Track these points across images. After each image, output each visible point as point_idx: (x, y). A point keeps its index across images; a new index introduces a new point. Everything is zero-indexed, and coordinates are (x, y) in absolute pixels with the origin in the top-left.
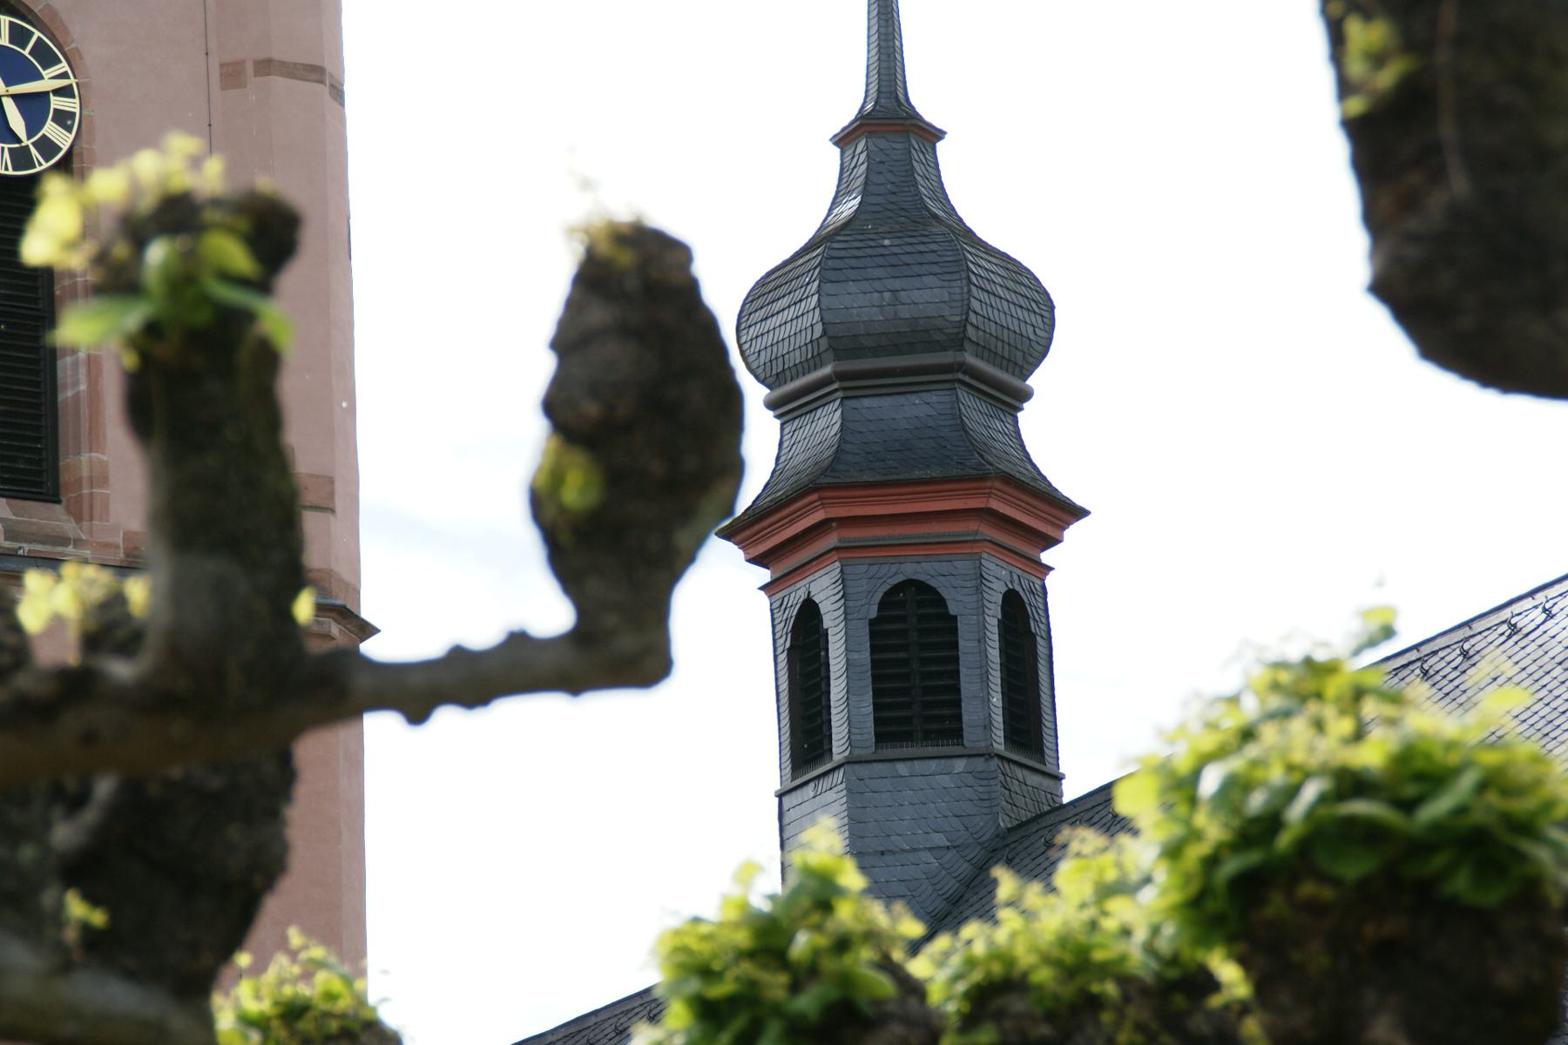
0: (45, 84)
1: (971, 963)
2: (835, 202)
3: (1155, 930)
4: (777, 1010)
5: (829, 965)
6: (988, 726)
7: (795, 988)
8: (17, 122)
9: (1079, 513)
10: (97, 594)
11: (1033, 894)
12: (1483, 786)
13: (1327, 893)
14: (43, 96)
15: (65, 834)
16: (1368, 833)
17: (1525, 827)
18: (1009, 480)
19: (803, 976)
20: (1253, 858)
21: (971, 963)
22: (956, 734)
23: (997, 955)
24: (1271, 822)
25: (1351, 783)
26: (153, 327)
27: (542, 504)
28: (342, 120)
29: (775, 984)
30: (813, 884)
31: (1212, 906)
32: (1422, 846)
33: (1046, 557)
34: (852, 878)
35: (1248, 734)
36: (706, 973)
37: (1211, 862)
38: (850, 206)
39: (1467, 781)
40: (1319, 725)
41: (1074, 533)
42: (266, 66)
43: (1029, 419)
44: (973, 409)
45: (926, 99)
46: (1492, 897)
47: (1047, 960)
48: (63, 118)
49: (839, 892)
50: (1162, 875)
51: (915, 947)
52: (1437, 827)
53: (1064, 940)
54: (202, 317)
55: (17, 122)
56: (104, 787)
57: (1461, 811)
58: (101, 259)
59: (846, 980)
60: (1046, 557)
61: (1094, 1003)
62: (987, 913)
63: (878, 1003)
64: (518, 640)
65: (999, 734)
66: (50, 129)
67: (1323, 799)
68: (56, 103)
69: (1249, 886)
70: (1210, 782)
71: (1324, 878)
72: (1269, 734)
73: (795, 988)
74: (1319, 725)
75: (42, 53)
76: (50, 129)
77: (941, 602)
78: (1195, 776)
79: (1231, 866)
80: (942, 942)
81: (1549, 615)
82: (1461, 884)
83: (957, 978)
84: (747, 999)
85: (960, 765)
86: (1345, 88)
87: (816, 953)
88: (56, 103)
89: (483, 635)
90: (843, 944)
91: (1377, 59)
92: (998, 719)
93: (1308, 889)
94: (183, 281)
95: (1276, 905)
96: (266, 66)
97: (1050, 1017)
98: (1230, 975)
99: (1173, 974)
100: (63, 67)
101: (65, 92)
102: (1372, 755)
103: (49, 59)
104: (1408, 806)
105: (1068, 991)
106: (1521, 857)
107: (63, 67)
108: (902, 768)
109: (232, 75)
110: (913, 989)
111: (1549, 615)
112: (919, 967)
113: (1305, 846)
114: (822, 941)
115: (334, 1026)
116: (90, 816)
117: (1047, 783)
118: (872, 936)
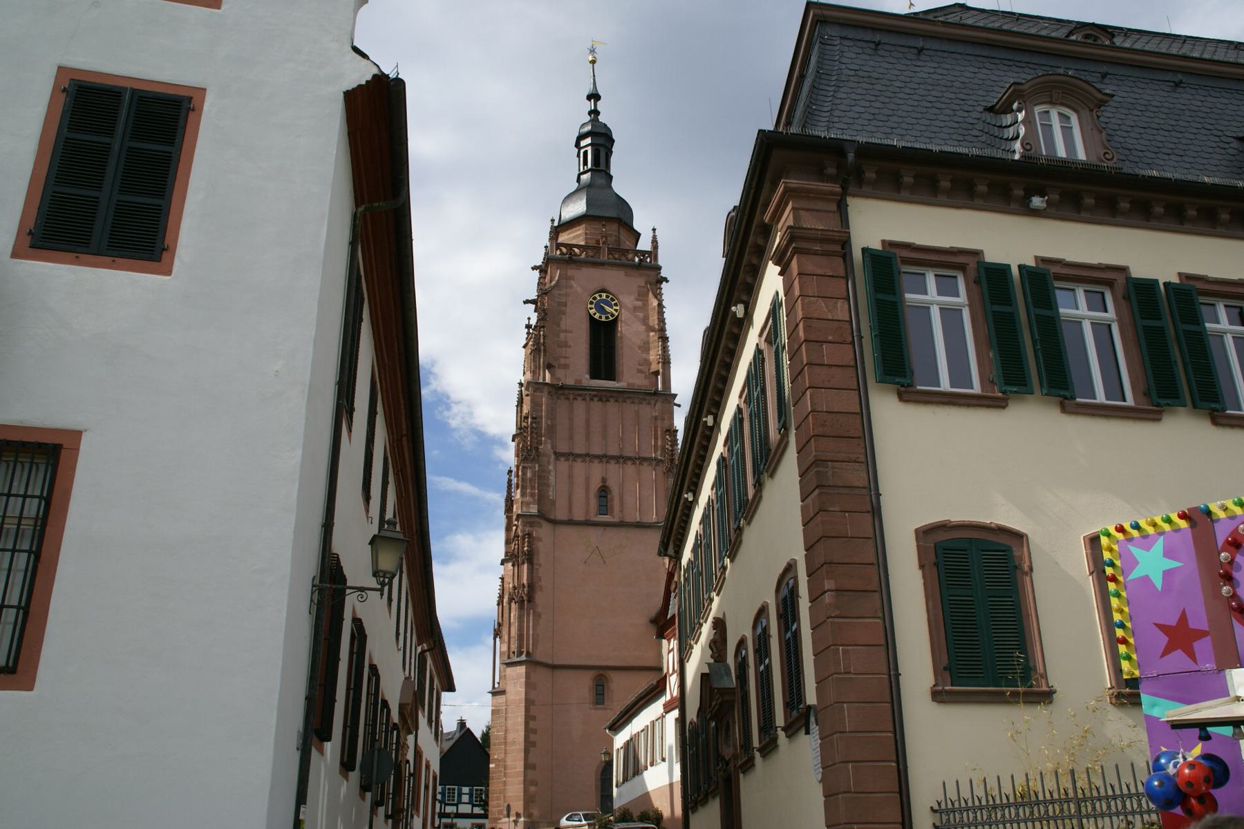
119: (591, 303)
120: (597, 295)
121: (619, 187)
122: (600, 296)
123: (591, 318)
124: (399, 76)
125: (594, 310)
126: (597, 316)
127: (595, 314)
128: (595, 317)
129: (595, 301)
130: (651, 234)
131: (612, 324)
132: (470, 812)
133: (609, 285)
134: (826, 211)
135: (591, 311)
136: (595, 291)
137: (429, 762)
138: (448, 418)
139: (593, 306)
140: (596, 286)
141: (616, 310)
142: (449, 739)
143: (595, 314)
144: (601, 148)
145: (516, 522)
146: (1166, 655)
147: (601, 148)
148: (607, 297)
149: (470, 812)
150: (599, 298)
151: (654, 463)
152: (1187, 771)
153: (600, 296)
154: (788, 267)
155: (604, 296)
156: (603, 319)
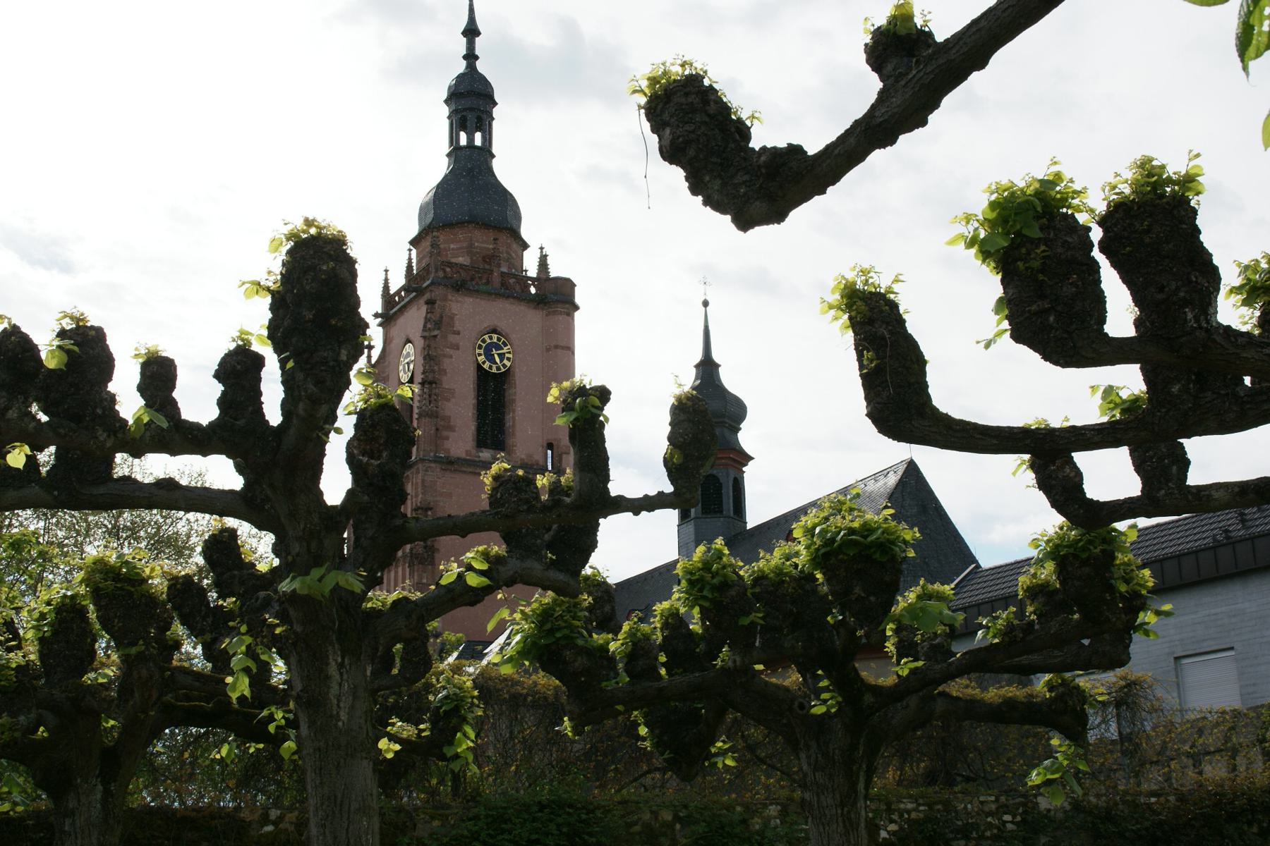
0: (505, 350)
1: (754, 572)
2: (695, 381)
3: (804, 566)
4: (708, 583)
5: (721, 572)
6: (729, 510)
7: (713, 577)
8: (498, 360)
9: (752, 458)
10: (553, 480)
11: (768, 556)
12: (883, 533)
13: (846, 558)
14: (504, 354)
15: (547, 537)
16: (855, 543)
17: (893, 543)
18: (735, 449)
19: (715, 575)
20: (829, 549)
21: (754, 572)
22: (721, 512)
23: (760, 570)
24: (833, 540)
25: (852, 531)
26: (576, 419)
27: (667, 462)
28: (574, 359)
29: (708, 576)
30: (717, 552)
31: (817, 560)
32: (868, 546)
33: (744, 469)
34: (726, 552)
35: (827, 519)
36: (691, 573)
37: (817, 550)
38: (699, 382)
39: (880, 531)
40: (844, 518)
41: (751, 463)
42: (556, 347)
43: (741, 436)
44: (727, 433)
45: (716, 357)
46: (884, 559)
47: (772, 571)
48: (508, 359)
49: (724, 555)
50: (804, 552)
51: (741, 568)
52: (872, 542)
53: (776, 567)
54: (588, 416)
55: (498, 360)
56: (555, 527)
57: (878, 539)
58: (564, 401)
59: (725, 576)
60: (744, 469)
61: (783, 582)
62: (758, 560)
63: (732, 581)
64: (661, 494)
65: (732, 513)
66: (505, 362)
67: (844, 535)
68: (507, 355)
69: (826, 556)
70: (817, 530)
71: (844, 554)
72: (832, 519)
73: (713, 577)
74: (844, 518)
75: (504, 343)
76: (505, 362)
77: (718, 479)
78: (814, 528)
79: (823, 551)
80: (747, 567)
81: (866, 486)
82: (877, 556)
83: (750, 576)
84: (701, 580)
85: (722, 519)
86: (861, 367)
87: (718, 569)
88: (507, 355)
89: (652, 492)
90: (724, 567)
91: (871, 361)
92: (732, 508)
93: (841, 556)
94: (584, 407)
95: (833, 560)
96: (556, 347)
97: (773, 585)
98: (819, 576)
99: (802, 575)
100: (509, 347)
101: (509, 353)
102: (856, 525)
103: (506, 345)
104: (865, 537)
105: (777, 579)
106: (892, 550)
107: (509, 347)
108: (708, 520)
109: (548, 350)
110: (741, 578)
111: (866, 486)
112: (742, 573)
113: (840, 546)
114: (720, 566)
115: (596, 583)
116: (551, 533)
117: (743, 524)
118: (731, 565)
119: (480, 347)
120: (486, 337)
122: (491, 338)
123: (479, 367)
124: (554, 272)
125: (483, 357)
126: (486, 366)
127: (484, 363)
128: (485, 366)
129: (484, 345)
130: (1122, 386)
131: (503, 378)
133: (502, 325)
135: (479, 358)
137: (546, 256)
138: (445, 356)
142: (339, 701)
143: (484, 363)
148: (499, 339)
152: (830, 597)
153: (491, 338)
154: (425, 229)
155: (495, 336)
156: (494, 370)
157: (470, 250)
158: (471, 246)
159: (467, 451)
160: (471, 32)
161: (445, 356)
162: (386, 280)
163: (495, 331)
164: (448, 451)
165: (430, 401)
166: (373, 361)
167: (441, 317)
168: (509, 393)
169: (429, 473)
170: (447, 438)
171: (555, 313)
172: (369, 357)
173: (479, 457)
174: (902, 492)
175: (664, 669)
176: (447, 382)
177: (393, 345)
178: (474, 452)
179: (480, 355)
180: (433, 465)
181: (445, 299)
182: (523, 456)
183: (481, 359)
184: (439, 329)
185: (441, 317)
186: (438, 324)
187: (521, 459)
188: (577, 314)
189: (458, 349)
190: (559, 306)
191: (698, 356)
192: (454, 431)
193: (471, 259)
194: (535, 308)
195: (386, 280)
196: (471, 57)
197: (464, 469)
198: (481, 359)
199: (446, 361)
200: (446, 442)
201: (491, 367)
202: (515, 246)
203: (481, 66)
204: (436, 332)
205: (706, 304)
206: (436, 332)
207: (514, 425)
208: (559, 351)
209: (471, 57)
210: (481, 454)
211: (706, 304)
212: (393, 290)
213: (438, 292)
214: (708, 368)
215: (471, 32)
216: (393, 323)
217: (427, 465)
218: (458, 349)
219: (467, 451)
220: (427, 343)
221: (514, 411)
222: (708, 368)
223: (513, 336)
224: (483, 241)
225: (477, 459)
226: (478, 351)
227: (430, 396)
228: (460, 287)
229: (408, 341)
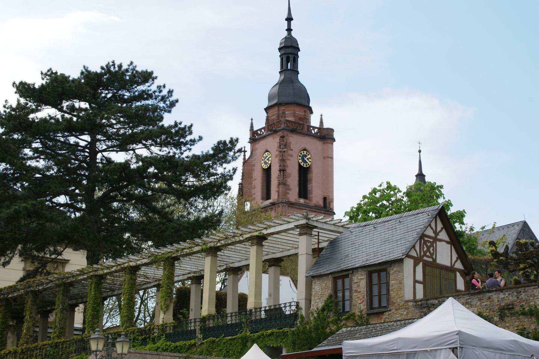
42: (328, 157)
45: (424, 172)
55: (307, 161)
96: (328, 157)
103: (308, 155)
119: (300, 156)
120: (302, 152)
121: (302, 78)
122: (304, 152)
124: (325, 126)
125: (301, 160)
126: (302, 164)
127: (301, 163)
129: (301, 155)
132: (377, 296)
133: (308, 148)
134: (440, 275)
136: (301, 150)
138: (287, 159)
139: (300, 158)
140: (303, 146)
141: (310, 162)
143: (301, 163)
144: (290, 55)
145: (37, 329)
146: (297, 284)
147: (290, 55)
148: (307, 153)
149: (377, 296)
150: (303, 154)
151: (517, 309)
153: (304, 152)
155: (305, 152)
156: (305, 166)
157: (294, 115)
158: (295, 113)
159: (295, 199)
160: (289, 19)
161: (287, 159)
162: (252, 124)
163: (305, 150)
164: (289, 199)
165: (283, 178)
166: (247, 157)
167: (286, 143)
168: (309, 176)
169: (284, 208)
170: (288, 194)
171: (327, 143)
172: (245, 156)
173: (300, 202)
174: (523, 233)
175: (68, 254)
176: (288, 170)
177: (257, 152)
178: (298, 200)
179: (300, 159)
180: (285, 205)
181: (287, 136)
182: (315, 202)
183: (300, 161)
184: (286, 148)
185: (286, 143)
186: (285, 146)
187: (315, 203)
188: (334, 143)
189: (292, 157)
190: (329, 140)
191: (417, 172)
192: (291, 191)
193: (295, 118)
194: (319, 140)
195: (252, 124)
196: (289, 30)
197: (296, 207)
198: (300, 161)
199: (288, 161)
200: (288, 195)
201: (309, 164)
202: (309, 112)
203: (293, 34)
204: (285, 150)
205: (420, 151)
206: (285, 150)
207: (312, 189)
208: (329, 159)
209: (289, 30)
210: (300, 200)
211: (420, 151)
212: (255, 129)
213: (286, 133)
214: (420, 176)
215: (289, 19)
216: (257, 142)
217: (283, 204)
218: (292, 157)
219: (295, 199)
220: (281, 154)
221: (312, 183)
222: (420, 176)
223: (311, 153)
224: (300, 112)
225: (299, 203)
226: (299, 158)
227: (283, 176)
228: (293, 131)
229: (267, 151)
